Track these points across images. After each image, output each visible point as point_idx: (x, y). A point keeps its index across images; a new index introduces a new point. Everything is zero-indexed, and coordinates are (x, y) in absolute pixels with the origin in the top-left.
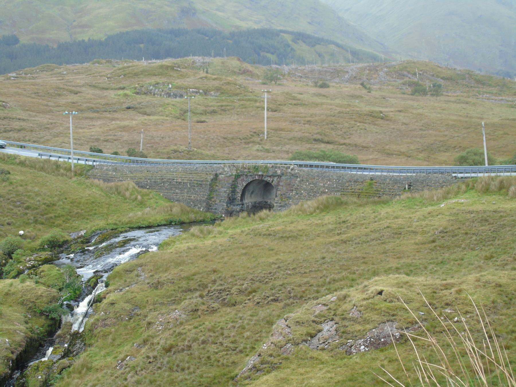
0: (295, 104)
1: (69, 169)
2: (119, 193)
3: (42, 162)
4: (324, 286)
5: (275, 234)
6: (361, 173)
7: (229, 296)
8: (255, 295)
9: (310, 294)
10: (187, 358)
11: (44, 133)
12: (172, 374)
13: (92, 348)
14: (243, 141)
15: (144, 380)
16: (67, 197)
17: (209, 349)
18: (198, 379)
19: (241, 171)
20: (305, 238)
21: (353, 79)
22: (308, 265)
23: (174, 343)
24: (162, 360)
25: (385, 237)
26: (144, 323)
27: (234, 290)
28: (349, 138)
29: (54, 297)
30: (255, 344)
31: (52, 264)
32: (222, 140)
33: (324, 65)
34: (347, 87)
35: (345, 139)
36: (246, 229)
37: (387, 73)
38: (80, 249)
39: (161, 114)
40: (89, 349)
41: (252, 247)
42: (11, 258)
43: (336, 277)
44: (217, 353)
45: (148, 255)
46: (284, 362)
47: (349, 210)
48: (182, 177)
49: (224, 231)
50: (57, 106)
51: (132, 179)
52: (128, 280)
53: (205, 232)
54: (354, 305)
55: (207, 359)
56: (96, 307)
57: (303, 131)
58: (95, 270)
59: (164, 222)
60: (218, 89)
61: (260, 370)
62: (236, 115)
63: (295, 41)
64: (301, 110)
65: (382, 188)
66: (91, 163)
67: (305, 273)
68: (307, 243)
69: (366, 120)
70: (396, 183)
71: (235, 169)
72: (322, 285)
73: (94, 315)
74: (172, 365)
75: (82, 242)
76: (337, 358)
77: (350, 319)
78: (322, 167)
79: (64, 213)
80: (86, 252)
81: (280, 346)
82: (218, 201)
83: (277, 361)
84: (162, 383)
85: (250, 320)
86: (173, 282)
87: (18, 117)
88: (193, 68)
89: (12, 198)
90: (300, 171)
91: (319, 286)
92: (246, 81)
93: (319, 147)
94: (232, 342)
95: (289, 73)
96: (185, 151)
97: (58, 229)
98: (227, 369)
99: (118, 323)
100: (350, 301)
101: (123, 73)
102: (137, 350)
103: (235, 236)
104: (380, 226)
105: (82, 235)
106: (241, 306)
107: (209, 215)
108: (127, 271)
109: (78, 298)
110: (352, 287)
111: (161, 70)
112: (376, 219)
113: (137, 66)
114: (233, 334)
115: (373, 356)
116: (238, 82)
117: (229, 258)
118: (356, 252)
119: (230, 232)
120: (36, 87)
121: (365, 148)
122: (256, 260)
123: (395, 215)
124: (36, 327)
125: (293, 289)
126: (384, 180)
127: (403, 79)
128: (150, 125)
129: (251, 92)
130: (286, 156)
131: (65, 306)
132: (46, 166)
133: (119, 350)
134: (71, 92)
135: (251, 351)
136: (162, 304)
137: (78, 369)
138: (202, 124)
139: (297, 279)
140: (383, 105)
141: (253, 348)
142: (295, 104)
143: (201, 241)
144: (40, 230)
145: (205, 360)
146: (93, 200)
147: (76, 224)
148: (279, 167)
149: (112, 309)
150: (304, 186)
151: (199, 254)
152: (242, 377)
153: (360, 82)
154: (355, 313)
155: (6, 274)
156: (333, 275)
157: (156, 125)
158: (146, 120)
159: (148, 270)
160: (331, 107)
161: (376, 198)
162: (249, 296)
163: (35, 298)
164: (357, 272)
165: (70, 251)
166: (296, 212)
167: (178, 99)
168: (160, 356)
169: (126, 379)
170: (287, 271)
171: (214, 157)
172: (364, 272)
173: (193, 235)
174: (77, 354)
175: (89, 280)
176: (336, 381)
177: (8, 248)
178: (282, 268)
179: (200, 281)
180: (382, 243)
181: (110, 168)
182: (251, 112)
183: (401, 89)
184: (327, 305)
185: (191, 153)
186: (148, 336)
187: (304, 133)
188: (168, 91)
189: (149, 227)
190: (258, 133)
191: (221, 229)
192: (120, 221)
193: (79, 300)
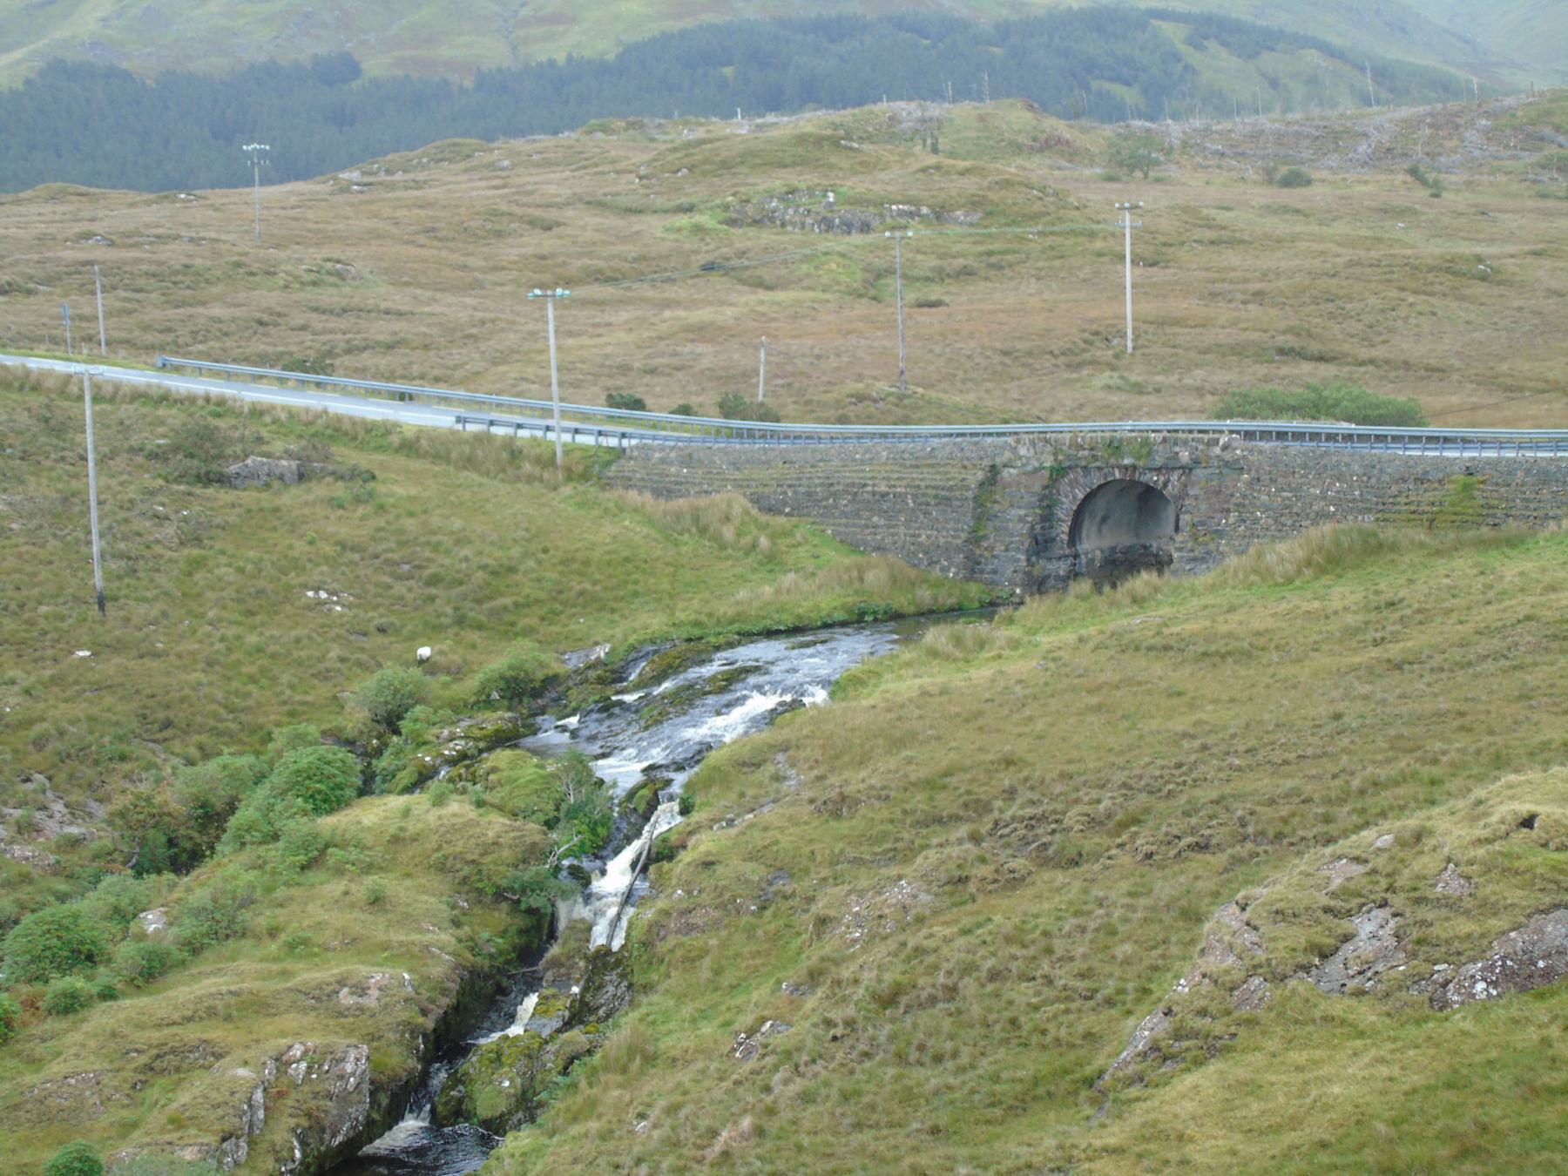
0: (1212, 242)
1: (547, 461)
2: (703, 531)
3: (466, 442)
4: (1345, 801)
5: (1183, 645)
6: (1437, 454)
7: (1058, 837)
8: (1136, 833)
9: (1305, 828)
10: (947, 1024)
11: (463, 351)
12: (906, 1071)
13: (655, 998)
14: (1062, 360)
15: (823, 1091)
16: (548, 545)
17: (1014, 995)
18: (986, 1087)
19: (1068, 457)
20: (1275, 657)
21: (1384, 156)
22: (1293, 737)
23: (904, 979)
24: (871, 1030)
25: (1523, 649)
26: (808, 919)
27: (1072, 817)
28: (1384, 342)
29: (534, 845)
30: (1150, 980)
31: (516, 746)
32: (997, 359)
33: (1290, 116)
34: (1366, 183)
35: (1373, 346)
36: (1092, 630)
37: (1489, 135)
38: (596, 702)
39: (806, 283)
40: (644, 1000)
41: (1117, 687)
42: (397, 732)
43: (1383, 773)
44: (1036, 1008)
45: (801, 717)
46: (1243, 1032)
47: (1403, 567)
48: (889, 479)
49: (1026, 639)
50: (495, 269)
51: (741, 486)
52: (750, 792)
53: (970, 643)
54: (1449, 860)
55: (1008, 1027)
56: (660, 874)
57: (1242, 325)
58: (645, 764)
59: (839, 616)
60: (975, 203)
61: (1172, 1057)
62: (1033, 280)
63: (1195, 43)
64: (1232, 258)
65: (1501, 499)
66: (613, 442)
67: (1286, 762)
68: (1282, 673)
69: (1432, 284)
70: (1545, 482)
71: (1049, 448)
72: (1338, 798)
73: (654, 898)
74: (903, 1045)
75: (601, 681)
76: (1404, 1018)
77: (1439, 903)
78: (1315, 436)
79: (542, 595)
80: (617, 710)
81: (1228, 985)
82: (1000, 548)
83: (1224, 1028)
84: (879, 1100)
85: (1128, 907)
86: (887, 797)
87: (383, 306)
88: (892, 137)
89: (385, 551)
90: (1251, 451)
91: (1330, 801)
92: (1056, 173)
93: (1296, 371)
94: (1082, 976)
95: (1185, 144)
96: (890, 394)
97: (527, 643)
98: (1072, 1056)
99: (726, 921)
100: (1434, 849)
101: (685, 161)
102: (792, 1002)
103: (1061, 653)
104: (1503, 615)
105: (598, 658)
106: (1097, 867)
107: (974, 590)
108: (744, 764)
109: (602, 848)
110: (1433, 802)
111: (800, 150)
112: (1491, 594)
113: (726, 138)
114: (1081, 950)
115: (1514, 1012)
116: (1034, 178)
117: (1049, 719)
118: (1436, 695)
119: (1045, 640)
120: (431, 213)
121: (1436, 372)
122: (1133, 727)
123: (1547, 579)
124: (486, 935)
125: (1252, 813)
126: (1509, 473)
127: (1541, 149)
128: (774, 319)
129: (1078, 208)
130: (1198, 403)
131: (565, 873)
132: (480, 453)
133: (733, 1002)
134: (533, 223)
135: (1138, 1001)
136: (858, 862)
137: (617, 1059)
138: (933, 310)
139: (1264, 783)
140: (1481, 236)
141: (1146, 991)
142: (1212, 242)
143: (959, 670)
144: (474, 646)
145: (1003, 1030)
146: (626, 553)
147: (580, 625)
148: (1186, 442)
149: (707, 881)
150: (1264, 498)
151: (957, 709)
152: (1119, 1080)
153: (1406, 166)
154: (1449, 885)
155: (384, 781)
156: (1369, 769)
157: (795, 317)
158: (762, 303)
159: (806, 760)
160: (1321, 247)
161: (1485, 530)
162: (1119, 836)
163: (477, 851)
164: (1444, 759)
165: (566, 706)
166: (1241, 575)
167: (857, 238)
168: (865, 1018)
169: (767, 1089)
170: (1230, 759)
171: (980, 415)
172: (1468, 758)
173: (934, 653)
174: (608, 1016)
175: (632, 794)
176: (1405, 1087)
177: (386, 703)
178: (1215, 750)
179: (968, 792)
180: (1515, 668)
181: (673, 455)
182: (1081, 268)
183: (1534, 182)
184: (1366, 861)
185: (906, 401)
186: (823, 959)
187: (1245, 330)
188: (824, 213)
189: (797, 631)
190: (1106, 335)
191: (1014, 632)
192: (710, 615)
193: (604, 853)
